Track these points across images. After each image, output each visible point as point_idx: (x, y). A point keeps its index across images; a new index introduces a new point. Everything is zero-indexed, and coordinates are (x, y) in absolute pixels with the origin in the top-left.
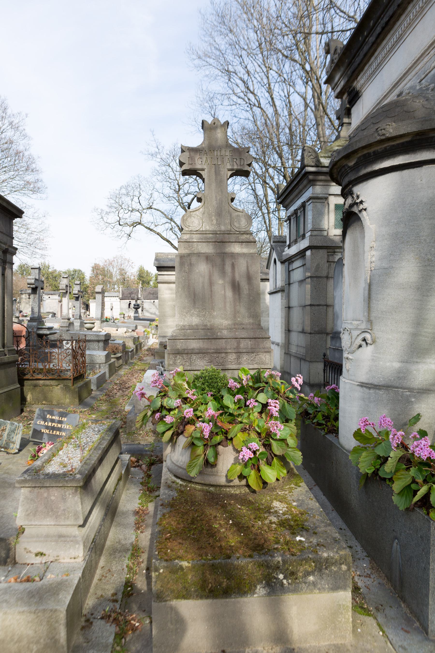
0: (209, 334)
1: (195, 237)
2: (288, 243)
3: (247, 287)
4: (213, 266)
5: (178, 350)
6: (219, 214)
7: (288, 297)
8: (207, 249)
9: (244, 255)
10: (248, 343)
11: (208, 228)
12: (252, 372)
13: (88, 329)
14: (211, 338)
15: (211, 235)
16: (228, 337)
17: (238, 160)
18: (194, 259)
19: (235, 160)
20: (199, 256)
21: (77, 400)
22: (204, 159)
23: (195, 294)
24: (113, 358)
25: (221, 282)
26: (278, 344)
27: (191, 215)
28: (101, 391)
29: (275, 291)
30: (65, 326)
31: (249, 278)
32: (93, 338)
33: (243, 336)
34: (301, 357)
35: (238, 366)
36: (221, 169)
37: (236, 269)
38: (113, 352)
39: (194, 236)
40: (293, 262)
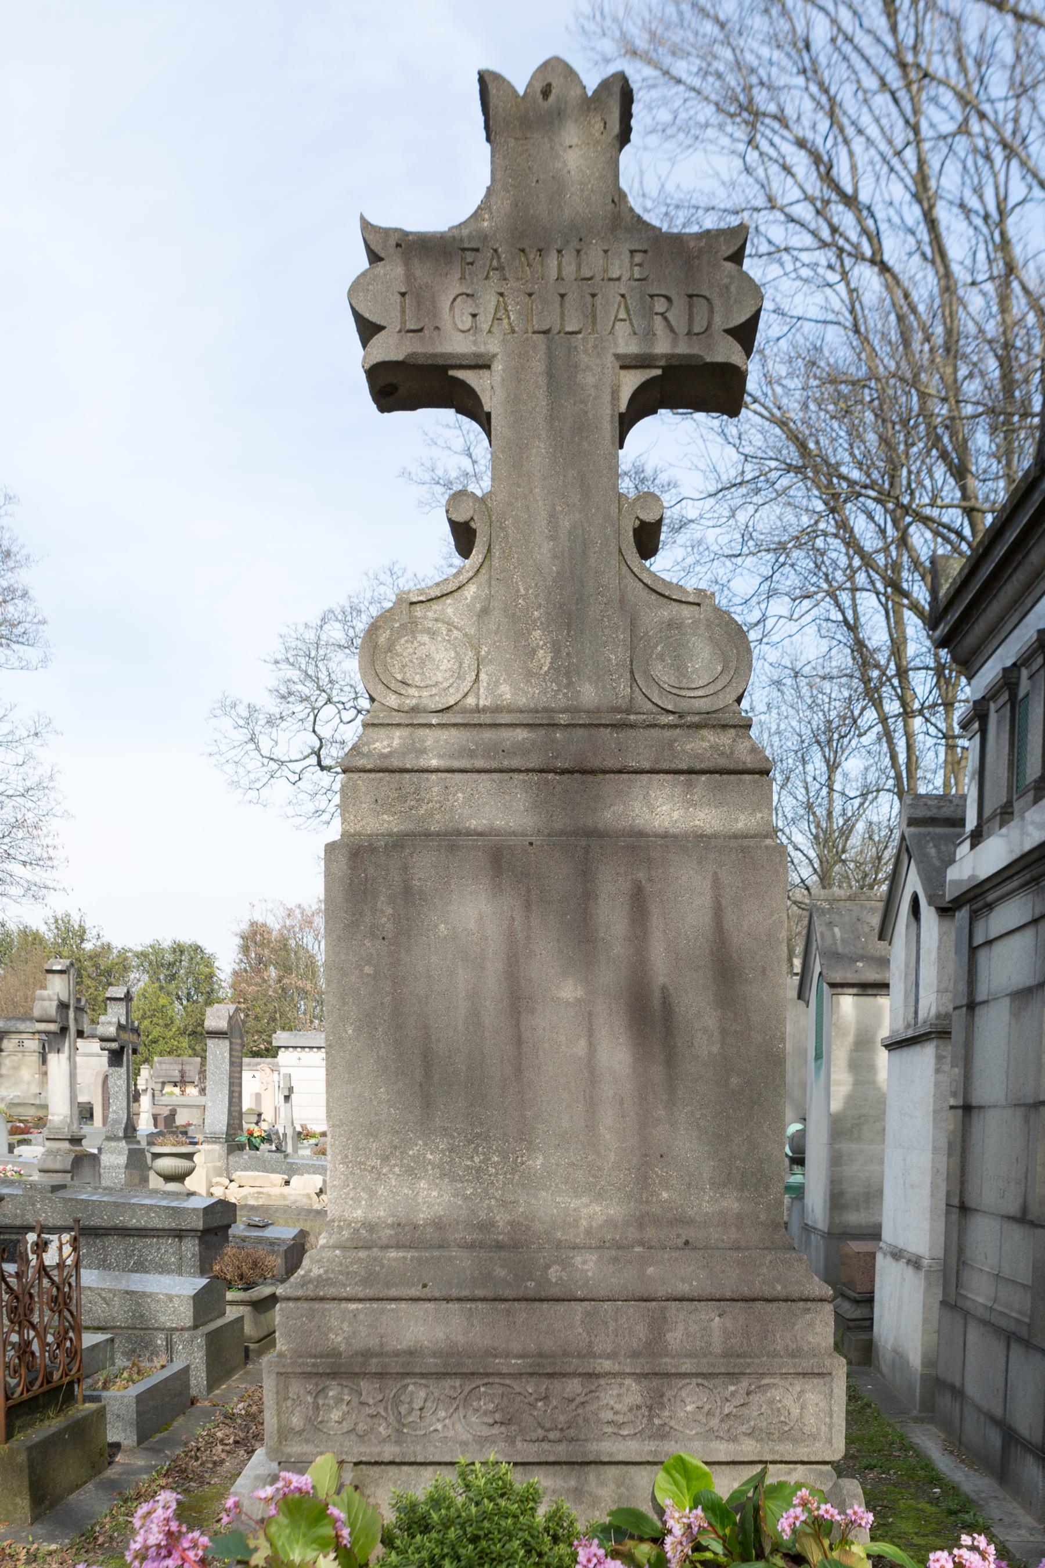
0: (500, 1272)
1: (437, 747)
2: (971, 823)
3: (710, 1020)
4: (528, 905)
5: (335, 1353)
6: (570, 612)
7: (967, 1060)
8: (498, 809)
9: (700, 842)
10: (715, 1326)
11: (506, 693)
12: (725, 1486)
13: (169, 1178)
14: (507, 1293)
15: (521, 734)
16: (602, 1293)
17: (680, 304)
18: (424, 866)
19: (660, 306)
20: (452, 848)
21: (23, 1503)
22: (490, 300)
23: (428, 1058)
24: (233, 1303)
25: (569, 991)
26: (915, 1263)
27: (414, 622)
28: (155, 1451)
29: (910, 1033)
30: (58, 1166)
31: (726, 970)
32: (156, 1222)
33: (684, 1288)
34: (1012, 1327)
35: (651, 1446)
36: (584, 359)
37: (656, 922)
38: (241, 1277)
39: (429, 738)
40: (990, 907)
